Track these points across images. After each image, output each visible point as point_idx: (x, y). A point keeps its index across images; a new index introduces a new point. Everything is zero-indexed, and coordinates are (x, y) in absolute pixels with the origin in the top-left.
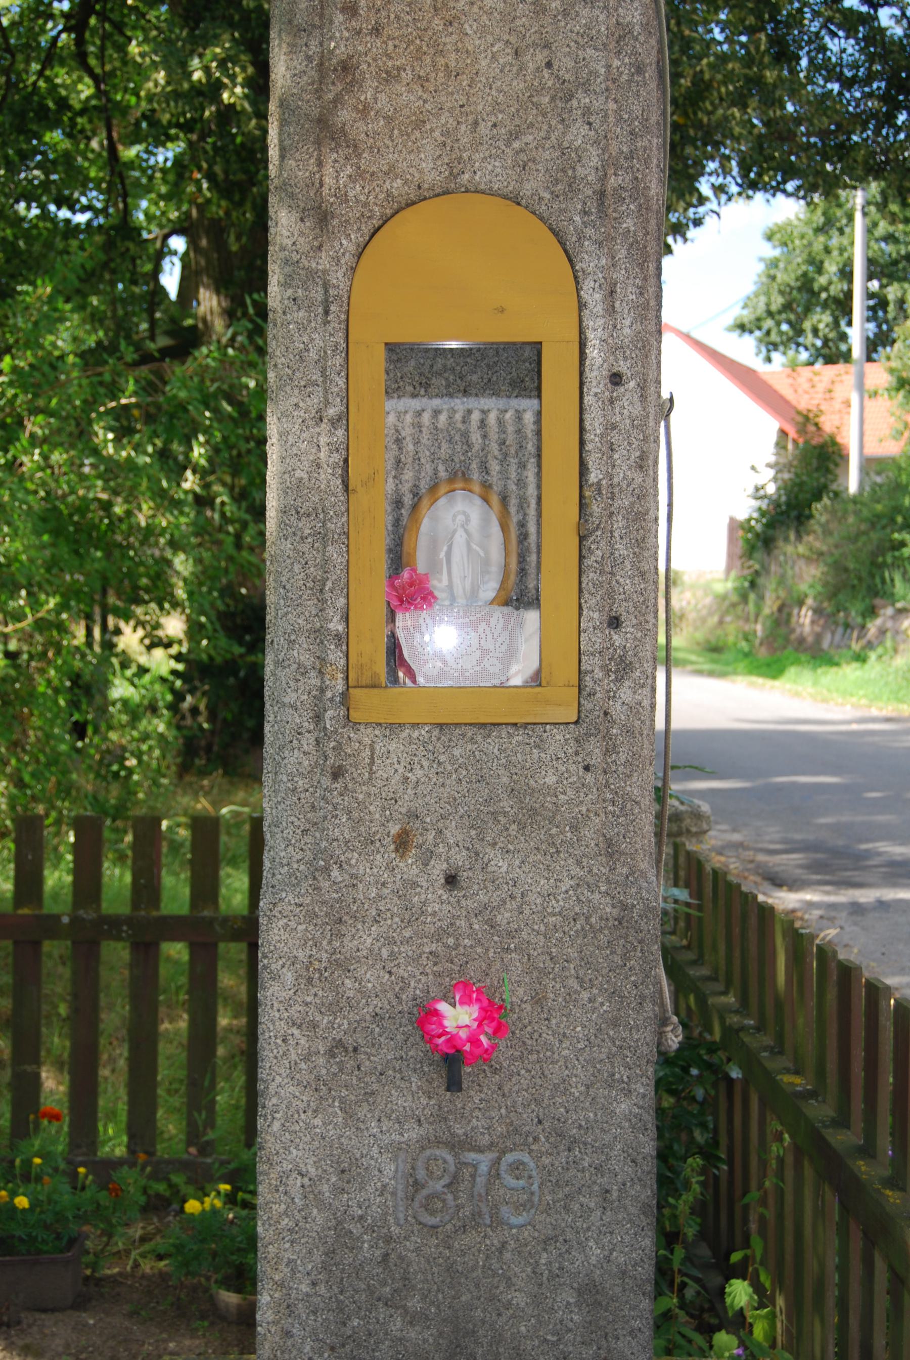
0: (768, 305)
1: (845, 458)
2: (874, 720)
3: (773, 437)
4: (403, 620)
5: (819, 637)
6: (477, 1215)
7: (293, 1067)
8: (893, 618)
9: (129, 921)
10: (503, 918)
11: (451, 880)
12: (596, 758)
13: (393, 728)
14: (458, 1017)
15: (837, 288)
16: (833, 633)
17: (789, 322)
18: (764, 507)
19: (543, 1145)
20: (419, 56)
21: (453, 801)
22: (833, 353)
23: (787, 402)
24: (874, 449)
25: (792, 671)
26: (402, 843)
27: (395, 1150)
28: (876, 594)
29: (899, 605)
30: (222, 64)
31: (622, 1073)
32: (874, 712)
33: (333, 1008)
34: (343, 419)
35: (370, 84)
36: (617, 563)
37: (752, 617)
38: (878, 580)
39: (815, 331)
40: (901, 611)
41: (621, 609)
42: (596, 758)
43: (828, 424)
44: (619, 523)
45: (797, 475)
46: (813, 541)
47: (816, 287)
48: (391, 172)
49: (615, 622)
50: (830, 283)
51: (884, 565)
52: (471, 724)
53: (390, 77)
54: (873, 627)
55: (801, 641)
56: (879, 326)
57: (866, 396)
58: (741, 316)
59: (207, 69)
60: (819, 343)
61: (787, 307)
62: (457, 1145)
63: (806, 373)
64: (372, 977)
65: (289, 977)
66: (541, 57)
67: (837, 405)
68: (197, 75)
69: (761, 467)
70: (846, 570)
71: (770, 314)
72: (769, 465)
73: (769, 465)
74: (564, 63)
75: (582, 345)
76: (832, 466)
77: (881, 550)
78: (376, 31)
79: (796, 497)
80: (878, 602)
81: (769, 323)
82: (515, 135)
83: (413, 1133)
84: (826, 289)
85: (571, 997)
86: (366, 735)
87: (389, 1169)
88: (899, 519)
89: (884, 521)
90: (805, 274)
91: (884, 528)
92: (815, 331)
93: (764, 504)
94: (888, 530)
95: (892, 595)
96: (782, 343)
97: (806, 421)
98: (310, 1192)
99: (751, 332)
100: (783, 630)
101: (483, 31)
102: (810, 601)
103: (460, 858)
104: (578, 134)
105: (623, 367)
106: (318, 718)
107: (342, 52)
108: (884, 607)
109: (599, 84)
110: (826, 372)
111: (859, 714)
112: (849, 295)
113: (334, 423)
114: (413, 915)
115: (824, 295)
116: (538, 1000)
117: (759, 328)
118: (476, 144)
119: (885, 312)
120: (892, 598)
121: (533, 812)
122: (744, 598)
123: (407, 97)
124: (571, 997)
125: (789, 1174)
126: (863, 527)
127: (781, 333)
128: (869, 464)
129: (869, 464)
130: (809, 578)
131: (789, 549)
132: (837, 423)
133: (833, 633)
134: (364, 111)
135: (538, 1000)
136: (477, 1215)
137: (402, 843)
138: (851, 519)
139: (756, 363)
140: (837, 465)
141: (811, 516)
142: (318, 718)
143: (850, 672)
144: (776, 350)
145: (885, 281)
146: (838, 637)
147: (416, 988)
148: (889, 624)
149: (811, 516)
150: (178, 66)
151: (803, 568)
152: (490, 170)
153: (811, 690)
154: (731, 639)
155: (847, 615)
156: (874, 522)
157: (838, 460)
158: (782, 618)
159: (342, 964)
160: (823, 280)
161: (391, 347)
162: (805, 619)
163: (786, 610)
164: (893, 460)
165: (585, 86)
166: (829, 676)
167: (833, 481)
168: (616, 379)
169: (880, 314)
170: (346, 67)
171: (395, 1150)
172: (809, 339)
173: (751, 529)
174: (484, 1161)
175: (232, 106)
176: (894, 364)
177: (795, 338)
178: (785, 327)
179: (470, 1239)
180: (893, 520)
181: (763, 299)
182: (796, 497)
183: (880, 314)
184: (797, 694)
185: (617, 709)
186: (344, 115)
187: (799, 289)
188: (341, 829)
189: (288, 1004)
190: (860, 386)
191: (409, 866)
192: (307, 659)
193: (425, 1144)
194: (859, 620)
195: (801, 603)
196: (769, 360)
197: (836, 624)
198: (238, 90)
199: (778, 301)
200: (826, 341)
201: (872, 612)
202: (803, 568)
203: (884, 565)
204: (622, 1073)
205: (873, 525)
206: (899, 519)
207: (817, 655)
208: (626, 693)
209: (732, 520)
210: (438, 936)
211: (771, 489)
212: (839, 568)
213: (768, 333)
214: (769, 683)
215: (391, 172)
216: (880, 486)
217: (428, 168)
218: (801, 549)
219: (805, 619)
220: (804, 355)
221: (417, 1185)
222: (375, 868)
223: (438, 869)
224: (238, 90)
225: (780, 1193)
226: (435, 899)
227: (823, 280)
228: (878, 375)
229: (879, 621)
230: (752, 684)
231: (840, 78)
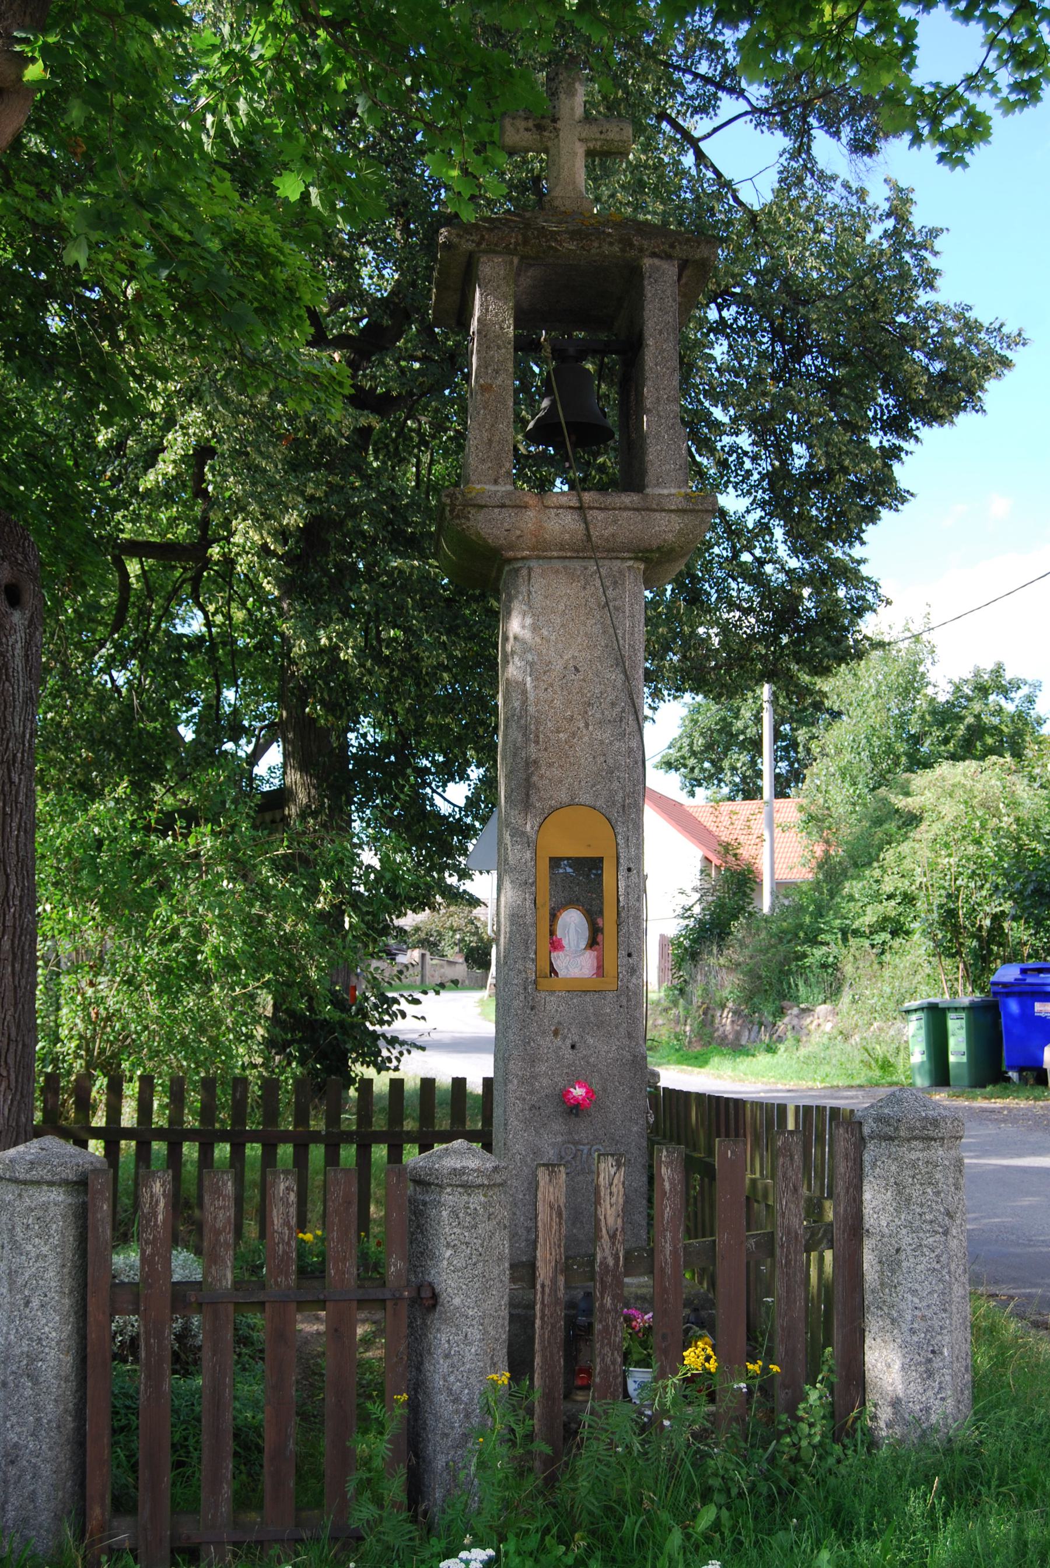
0: (691, 745)
1: (760, 884)
2: (778, 1091)
3: (699, 865)
4: (554, 954)
5: (738, 1035)
6: (583, 1169)
7: (517, 1114)
8: (797, 1016)
9: (356, 1133)
10: (592, 1060)
11: (573, 1047)
12: (624, 1003)
13: (552, 992)
14: (578, 1092)
15: (751, 732)
16: (750, 1031)
17: (712, 762)
18: (692, 924)
19: (606, 1143)
20: (560, 758)
21: (574, 1018)
22: (749, 791)
23: (710, 832)
24: (783, 875)
25: (715, 1060)
26: (556, 1033)
27: (553, 1145)
28: (784, 997)
29: (802, 1006)
30: (339, 635)
31: (634, 1116)
32: (780, 1086)
33: (532, 1093)
34: (534, 883)
35: (544, 768)
36: (630, 934)
37: (682, 1019)
38: (785, 986)
39: (733, 769)
40: (803, 1010)
41: (632, 950)
42: (624, 1003)
43: (745, 853)
44: (631, 920)
45: (719, 898)
46: (733, 954)
47: (734, 730)
48: (551, 798)
49: (629, 955)
50: (746, 728)
51: (790, 972)
52: (579, 990)
53: (550, 765)
54: (782, 1025)
55: (724, 1037)
56: (791, 765)
57: (777, 831)
58: (667, 754)
59: (330, 639)
60: (737, 780)
61: (709, 747)
62: (575, 1143)
63: (727, 807)
64: (545, 1082)
65: (515, 1082)
66: (602, 759)
67: (753, 839)
68: (324, 641)
69: (689, 891)
70: (760, 977)
71: (694, 753)
72: (695, 889)
73: (695, 889)
74: (610, 761)
75: (618, 858)
76: (748, 891)
77: (787, 961)
78: (546, 750)
79: (719, 918)
80: (785, 1003)
81: (692, 762)
82: (593, 786)
83: (559, 1139)
84: (743, 732)
85: (616, 1089)
86: (543, 994)
87: (552, 1152)
88: (802, 934)
89: (789, 937)
90: (723, 719)
91: (789, 942)
92: (733, 769)
93: (691, 923)
94: (792, 944)
95: (797, 997)
96: (705, 779)
97: (727, 849)
98: (523, 1161)
99: (677, 769)
100: (707, 1030)
101: (582, 750)
102: (730, 1004)
103: (576, 1038)
104: (615, 785)
105: (632, 866)
106: (525, 989)
107: (533, 757)
108: (791, 1008)
109: (622, 768)
110: (744, 807)
111: (768, 1087)
112: (761, 736)
113: (532, 885)
114: (559, 1059)
115: (741, 737)
116: (604, 1090)
117: (685, 766)
118: (580, 789)
119: (797, 753)
120: (796, 999)
121: (602, 1022)
122: (675, 1003)
123: (557, 772)
124: (616, 1089)
125: (699, 1204)
126: (773, 941)
127: (703, 770)
128: (781, 888)
129: (781, 888)
130: (728, 985)
131: (712, 961)
132: (753, 852)
133: (750, 1031)
134: (542, 777)
135: (604, 1090)
136: (583, 1169)
137: (556, 1033)
138: (763, 935)
139: (682, 797)
140: (753, 890)
141: (730, 933)
142: (525, 989)
143: (763, 1059)
144: (700, 785)
145: (794, 725)
146: (753, 1034)
147: (561, 1086)
148: (795, 1022)
149: (730, 933)
150: (311, 634)
151: (723, 977)
152: (585, 798)
153: (729, 1073)
154: (665, 1039)
155: (761, 1015)
156: (782, 937)
157: (755, 886)
158: (707, 1021)
159: (534, 1077)
160: (739, 724)
161: (551, 859)
162: (726, 1021)
163: (711, 1012)
164: (795, 883)
165: (618, 768)
166: (745, 1064)
167: (749, 904)
168: (629, 870)
169: (792, 754)
170: (535, 762)
171: (553, 1145)
172: (727, 776)
173: (680, 945)
174: (586, 1149)
175: (346, 661)
176: (805, 802)
177: (714, 777)
178: (707, 765)
179: (581, 1178)
180: (796, 935)
181: (686, 741)
182: (719, 918)
183: (792, 754)
184: (719, 1077)
185: (631, 985)
186: (535, 778)
187: (719, 731)
188: (534, 1027)
189: (515, 1091)
190: (771, 824)
191: (558, 1041)
192: (521, 968)
193: (564, 1143)
194: (771, 1019)
195: (723, 1007)
196: (692, 794)
197: (752, 1022)
198: (350, 651)
199: (700, 742)
200: (744, 778)
201: (781, 1012)
202: (723, 977)
203: (790, 972)
204: (634, 1116)
205: (781, 939)
206: (802, 934)
207: (736, 1048)
208: (634, 980)
209: (662, 936)
210: (569, 1066)
211: (697, 909)
212: (753, 975)
213: (692, 769)
214: (697, 1070)
215: (551, 798)
216: (788, 907)
217: (564, 796)
218: (722, 961)
219: (726, 1021)
220: (725, 790)
221: (562, 1158)
222: (547, 1042)
223: (569, 1042)
224: (350, 651)
225: (696, 1213)
226: (567, 1053)
227: (739, 724)
228: (788, 810)
229: (786, 1020)
230: (682, 1071)
231: (739, 608)
